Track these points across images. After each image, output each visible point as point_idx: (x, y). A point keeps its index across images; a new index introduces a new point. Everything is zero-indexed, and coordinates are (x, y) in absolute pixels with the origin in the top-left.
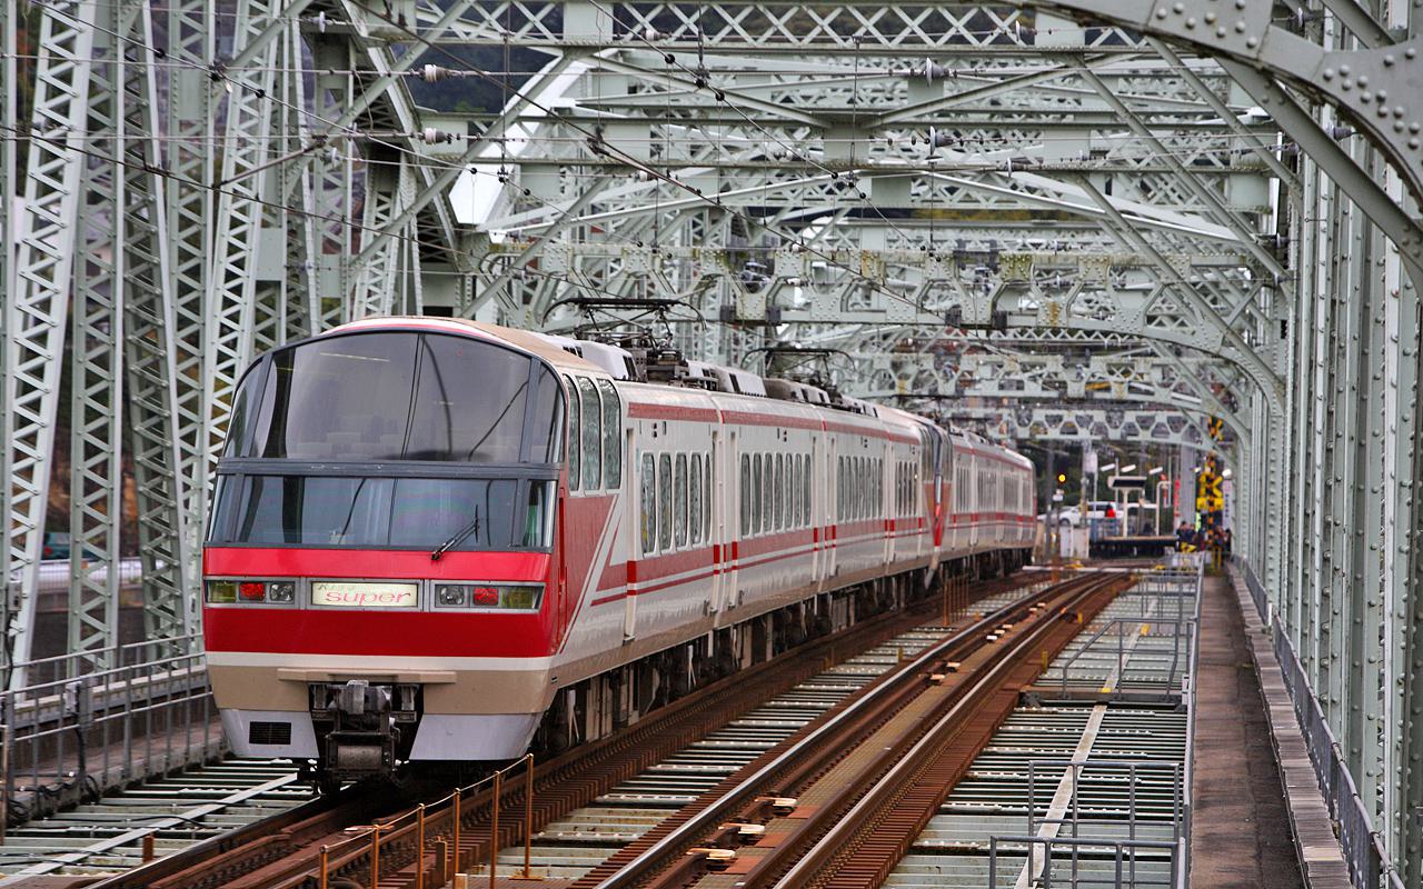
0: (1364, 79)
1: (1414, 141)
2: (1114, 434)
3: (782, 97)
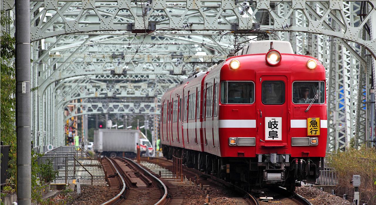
0: (369, 44)
1: (375, 51)
2: (137, 111)
3: (116, 49)
